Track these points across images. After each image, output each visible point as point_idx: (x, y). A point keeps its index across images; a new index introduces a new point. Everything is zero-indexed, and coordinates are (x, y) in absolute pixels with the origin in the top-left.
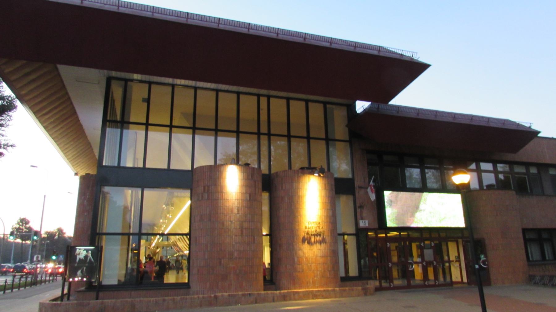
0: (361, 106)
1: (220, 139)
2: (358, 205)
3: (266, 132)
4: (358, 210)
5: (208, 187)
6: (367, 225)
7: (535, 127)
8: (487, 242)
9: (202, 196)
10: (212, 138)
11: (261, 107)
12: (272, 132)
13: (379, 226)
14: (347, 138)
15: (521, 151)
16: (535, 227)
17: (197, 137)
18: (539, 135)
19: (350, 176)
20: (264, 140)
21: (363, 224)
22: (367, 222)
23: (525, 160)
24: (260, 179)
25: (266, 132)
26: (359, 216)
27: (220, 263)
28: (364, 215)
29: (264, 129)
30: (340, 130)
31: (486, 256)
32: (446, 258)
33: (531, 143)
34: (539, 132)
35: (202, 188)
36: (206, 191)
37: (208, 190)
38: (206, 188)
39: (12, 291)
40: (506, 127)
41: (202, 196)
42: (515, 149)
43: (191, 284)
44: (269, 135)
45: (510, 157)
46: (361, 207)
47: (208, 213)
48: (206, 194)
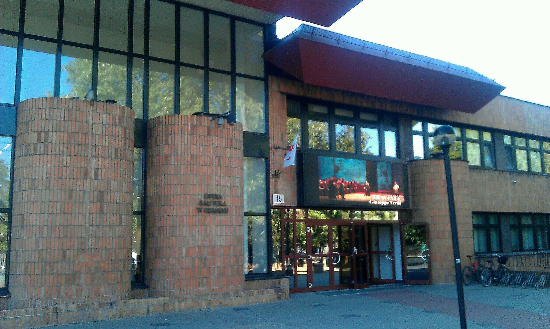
0: (286, 27)
1: (65, 60)
2: (272, 172)
3: (142, 53)
4: (272, 180)
5: (47, 133)
6: (283, 202)
7: (499, 81)
8: (431, 228)
9: (35, 149)
10: (52, 57)
11: (135, 20)
12: (151, 54)
13: (299, 202)
14: (262, 75)
15: (486, 108)
16: (484, 211)
17: (26, 53)
18: (501, 93)
19: (263, 131)
20: (138, 62)
21: (277, 199)
22: (283, 197)
23: (480, 123)
24: (132, 125)
25: (142, 53)
26: (272, 189)
27: (64, 255)
28: (280, 186)
29: (139, 48)
30: (251, 60)
31: (428, 247)
32: (374, 249)
33: (496, 100)
34: (502, 88)
35: (36, 135)
36: (42, 141)
37: (46, 139)
38: (43, 135)
39: (135, 213)
40: (468, 77)
41: (35, 149)
42: (473, 108)
43: (10, 289)
44: (146, 57)
45: (464, 117)
46: (276, 175)
47: (45, 176)
48: (42, 146)
